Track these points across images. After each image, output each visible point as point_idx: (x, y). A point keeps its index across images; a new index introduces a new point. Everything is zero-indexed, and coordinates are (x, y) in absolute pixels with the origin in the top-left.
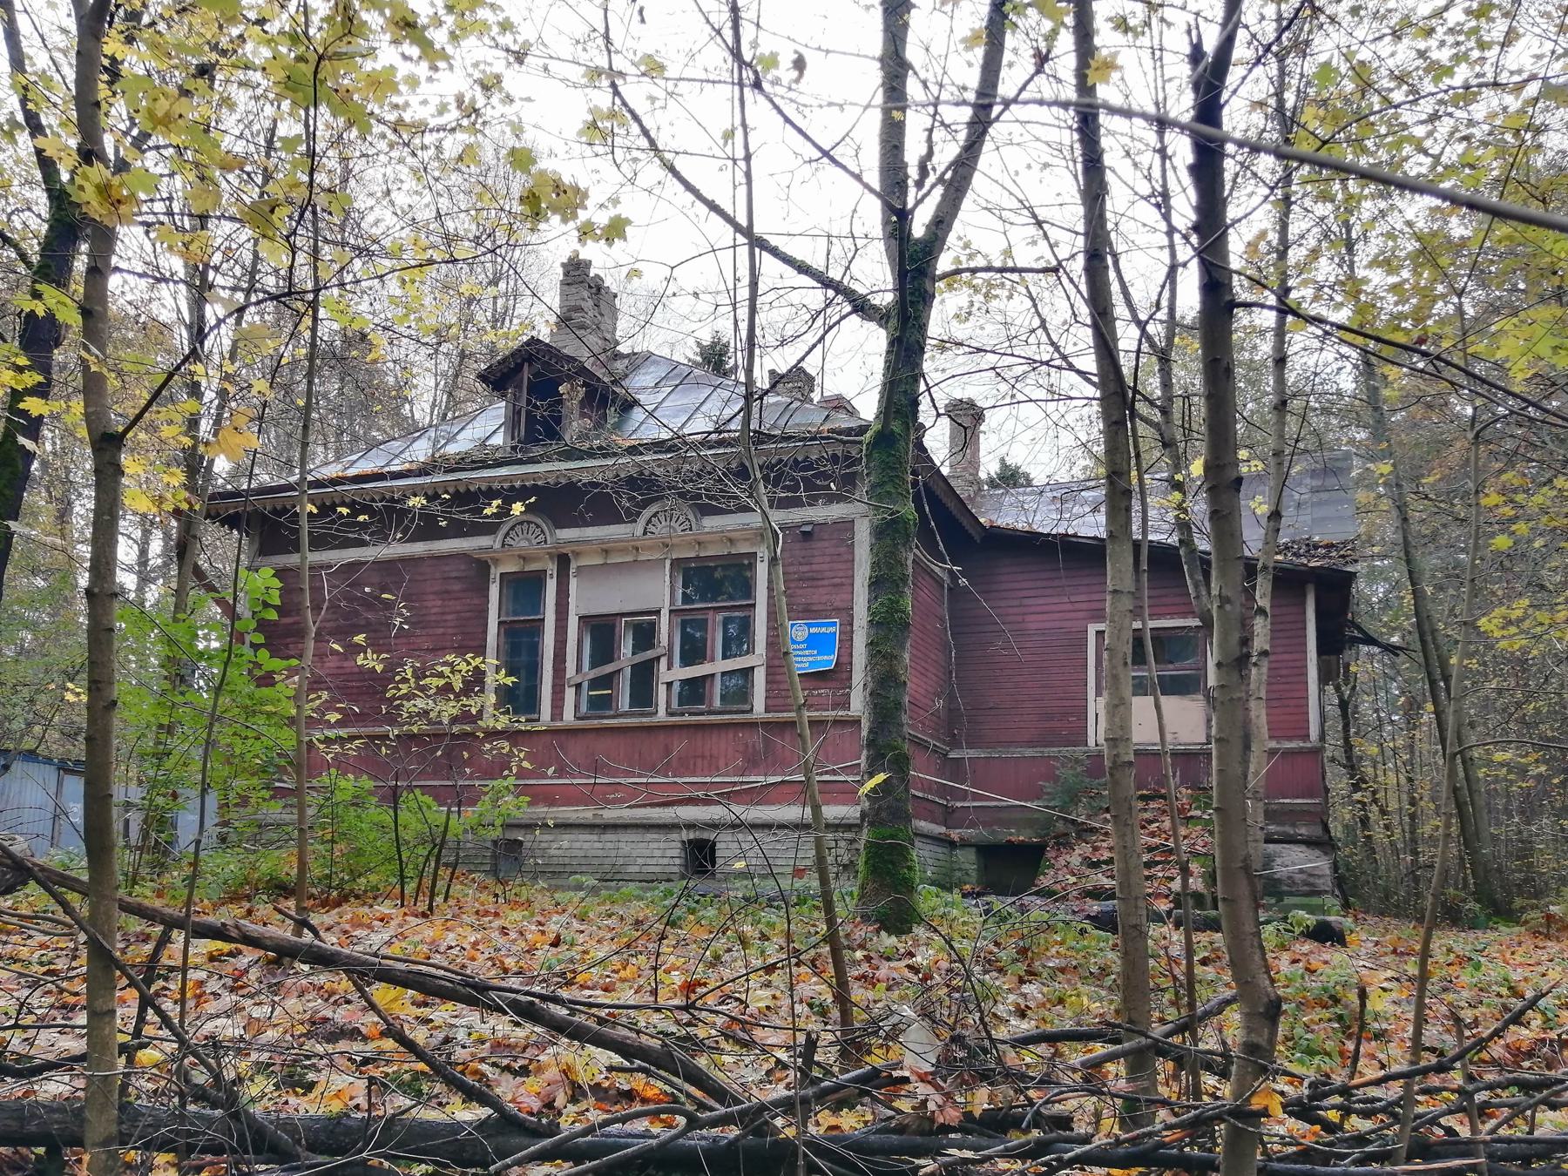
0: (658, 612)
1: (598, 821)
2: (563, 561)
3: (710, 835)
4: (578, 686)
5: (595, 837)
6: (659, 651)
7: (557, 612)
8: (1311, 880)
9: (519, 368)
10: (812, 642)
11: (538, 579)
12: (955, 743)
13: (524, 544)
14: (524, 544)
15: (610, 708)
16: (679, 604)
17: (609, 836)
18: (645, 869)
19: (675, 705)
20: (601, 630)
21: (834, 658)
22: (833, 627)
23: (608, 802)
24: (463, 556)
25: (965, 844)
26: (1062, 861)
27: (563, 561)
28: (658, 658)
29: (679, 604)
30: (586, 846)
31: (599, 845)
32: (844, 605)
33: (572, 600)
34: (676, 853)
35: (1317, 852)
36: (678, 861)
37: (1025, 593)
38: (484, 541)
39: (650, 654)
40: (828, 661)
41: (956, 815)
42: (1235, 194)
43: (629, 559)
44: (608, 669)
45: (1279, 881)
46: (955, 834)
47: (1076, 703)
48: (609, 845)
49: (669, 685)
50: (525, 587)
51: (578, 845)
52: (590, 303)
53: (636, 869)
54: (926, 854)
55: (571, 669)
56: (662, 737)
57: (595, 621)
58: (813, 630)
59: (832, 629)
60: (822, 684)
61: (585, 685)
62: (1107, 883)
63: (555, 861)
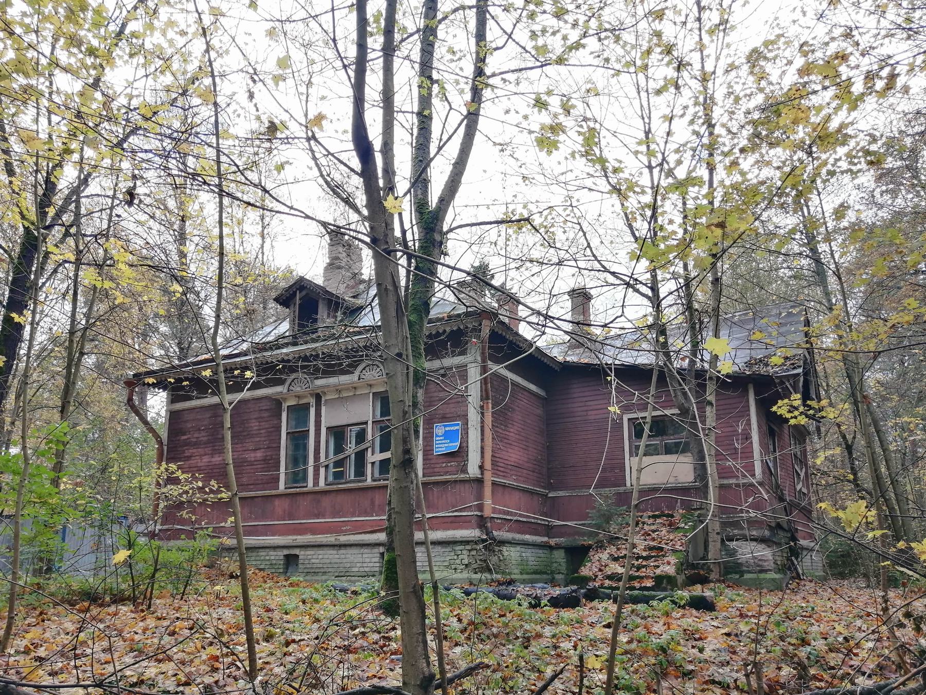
0: (366, 423)
1: (337, 543)
2: (318, 397)
3: (296, 551)
4: (327, 467)
5: (335, 552)
6: (368, 445)
7: (316, 426)
8: (760, 563)
9: (294, 294)
10: (447, 435)
11: (306, 407)
12: (551, 488)
13: (299, 389)
14: (299, 389)
15: (342, 478)
16: (378, 418)
17: (342, 551)
18: (362, 569)
19: (377, 475)
20: (338, 433)
21: (458, 444)
22: (457, 426)
23: (342, 531)
24: (267, 398)
25: (558, 547)
26: (596, 557)
27: (318, 397)
28: (367, 449)
29: (378, 418)
30: (331, 557)
31: (337, 556)
32: (463, 413)
33: (323, 419)
34: (377, 560)
35: (763, 546)
36: (378, 565)
37: (585, 399)
38: (279, 389)
39: (362, 447)
40: (455, 446)
41: (554, 530)
42: (911, 110)
43: (351, 394)
44: (341, 456)
45: (741, 564)
46: (553, 542)
47: (618, 461)
48: (343, 556)
49: (373, 463)
50: (300, 411)
51: (326, 556)
52: (344, 254)
53: (356, 569)
54: (528, 554)
55: (323, 458)
56: (370, 494)
57: (336, 429)
58: (447, 429)
59: (457, 428)
60: (452, 459)
61: (331, 465)
62: (620, 570)
63: (315, 566)
